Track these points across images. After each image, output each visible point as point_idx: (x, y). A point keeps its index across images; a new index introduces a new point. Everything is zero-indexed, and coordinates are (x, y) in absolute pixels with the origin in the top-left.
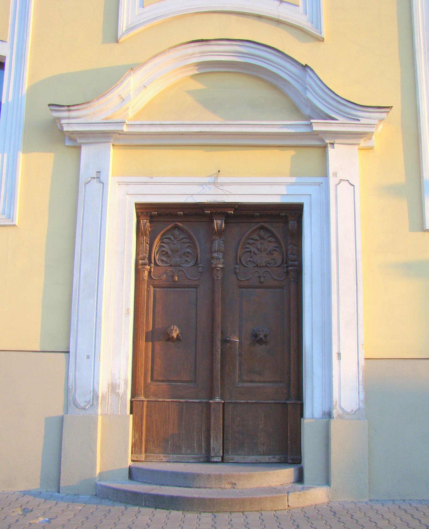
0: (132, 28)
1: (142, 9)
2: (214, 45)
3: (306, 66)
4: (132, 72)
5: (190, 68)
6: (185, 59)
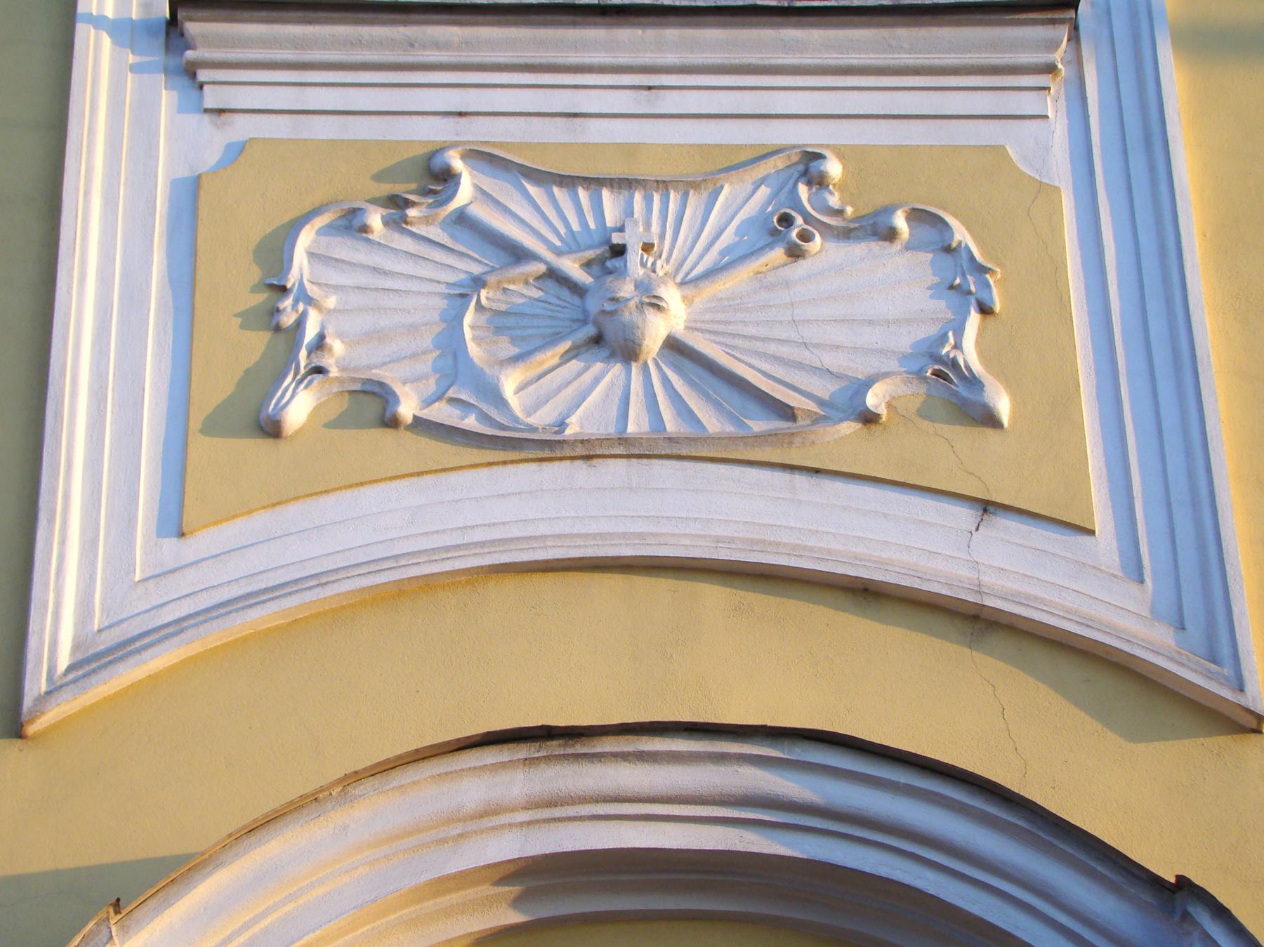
0: (110, 651)
1: (170, 545)
2: (616, 756)
3: (1183, 883)
4: (114, 919)
5: (471, 893)
6: (443, 841)
